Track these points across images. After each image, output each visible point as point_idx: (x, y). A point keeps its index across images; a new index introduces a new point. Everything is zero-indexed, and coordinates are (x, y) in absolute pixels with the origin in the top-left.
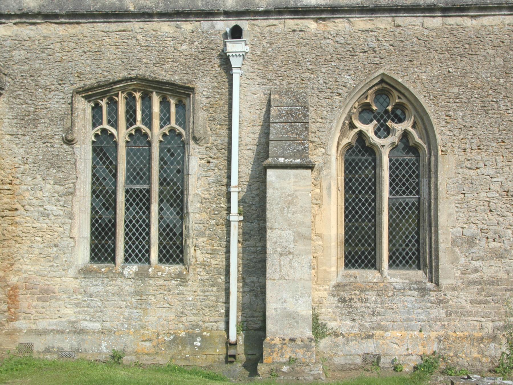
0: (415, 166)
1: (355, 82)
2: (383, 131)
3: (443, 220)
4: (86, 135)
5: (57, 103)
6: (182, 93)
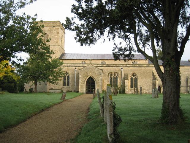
0: (136, 79)
1: (131, 73)
2: (134, 77)
3: (138, 84)
4: (109, 77)
5: (107, 74)
6: (118, 73)
